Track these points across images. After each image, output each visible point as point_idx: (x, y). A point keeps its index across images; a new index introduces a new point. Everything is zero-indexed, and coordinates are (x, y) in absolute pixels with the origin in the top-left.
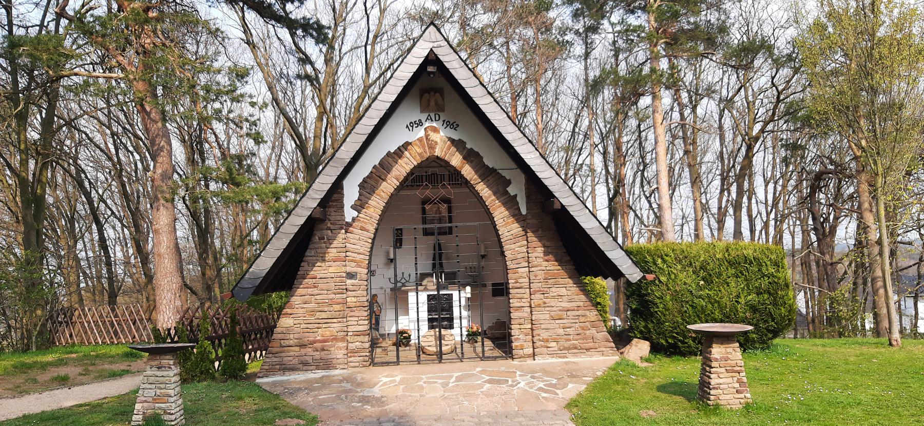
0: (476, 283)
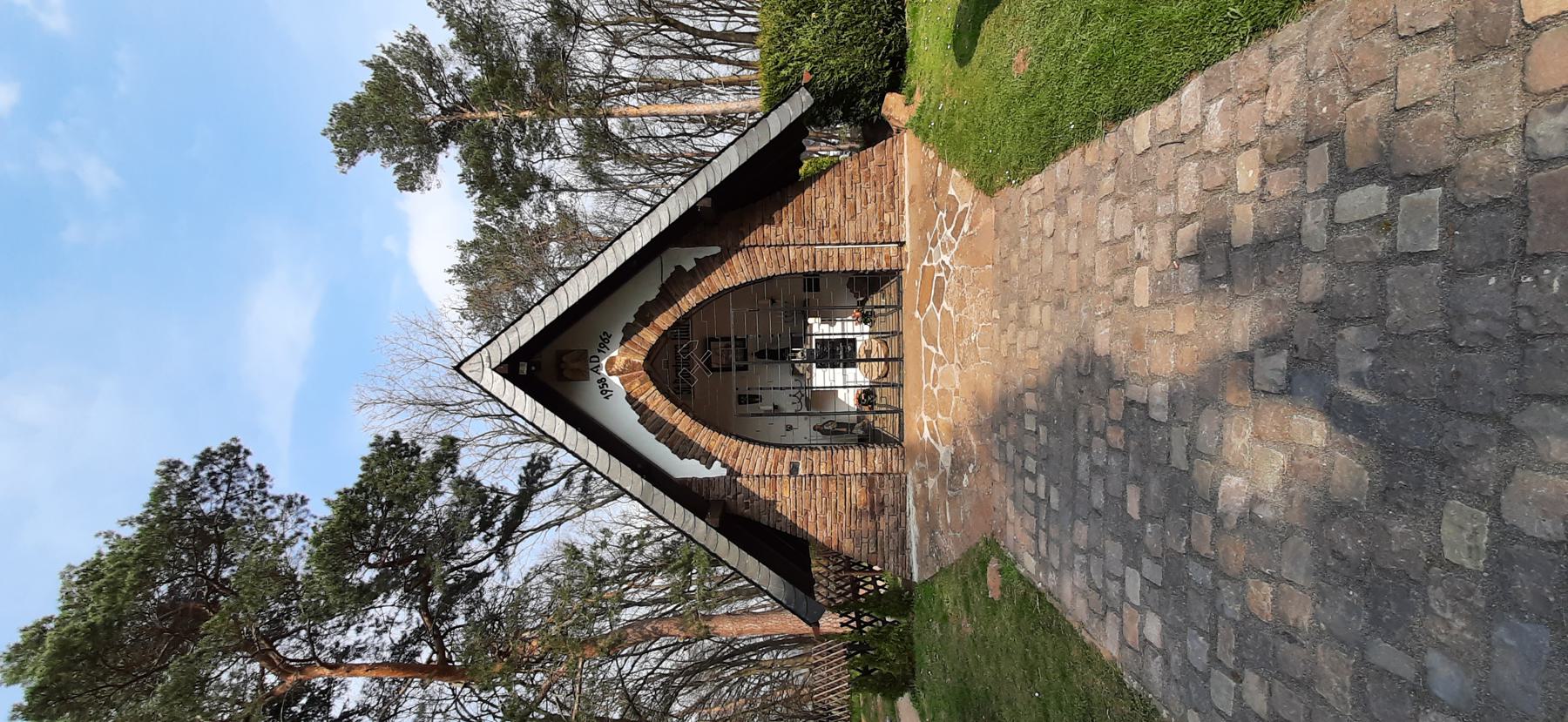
0: (804, 312)
